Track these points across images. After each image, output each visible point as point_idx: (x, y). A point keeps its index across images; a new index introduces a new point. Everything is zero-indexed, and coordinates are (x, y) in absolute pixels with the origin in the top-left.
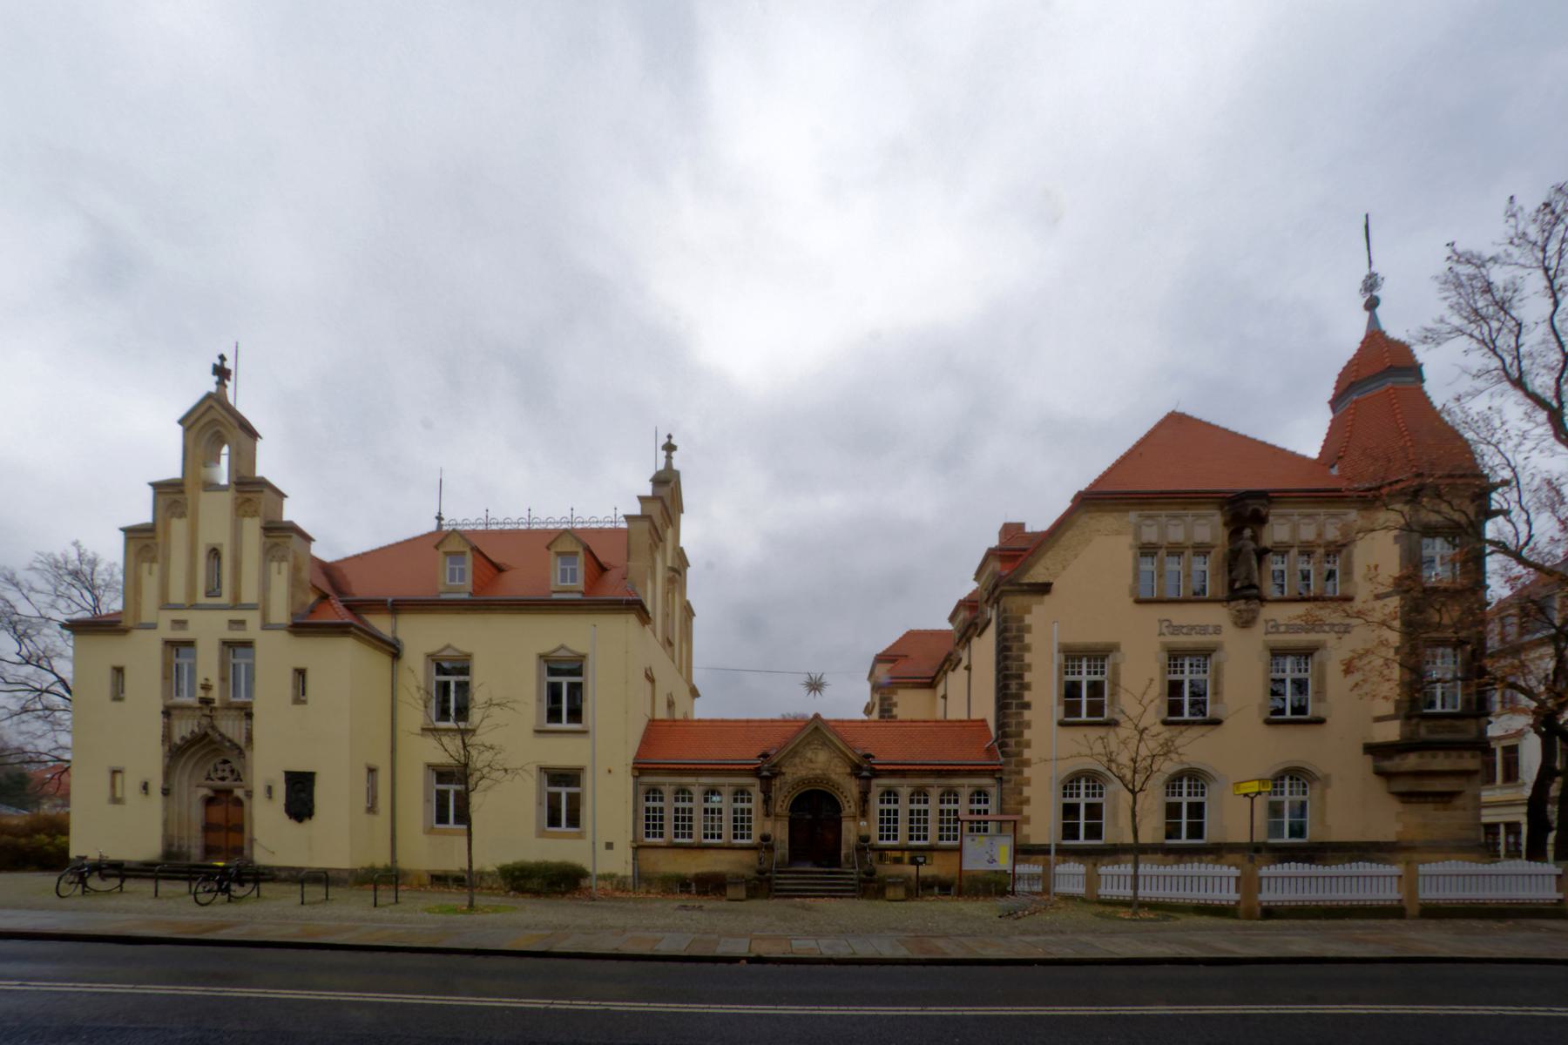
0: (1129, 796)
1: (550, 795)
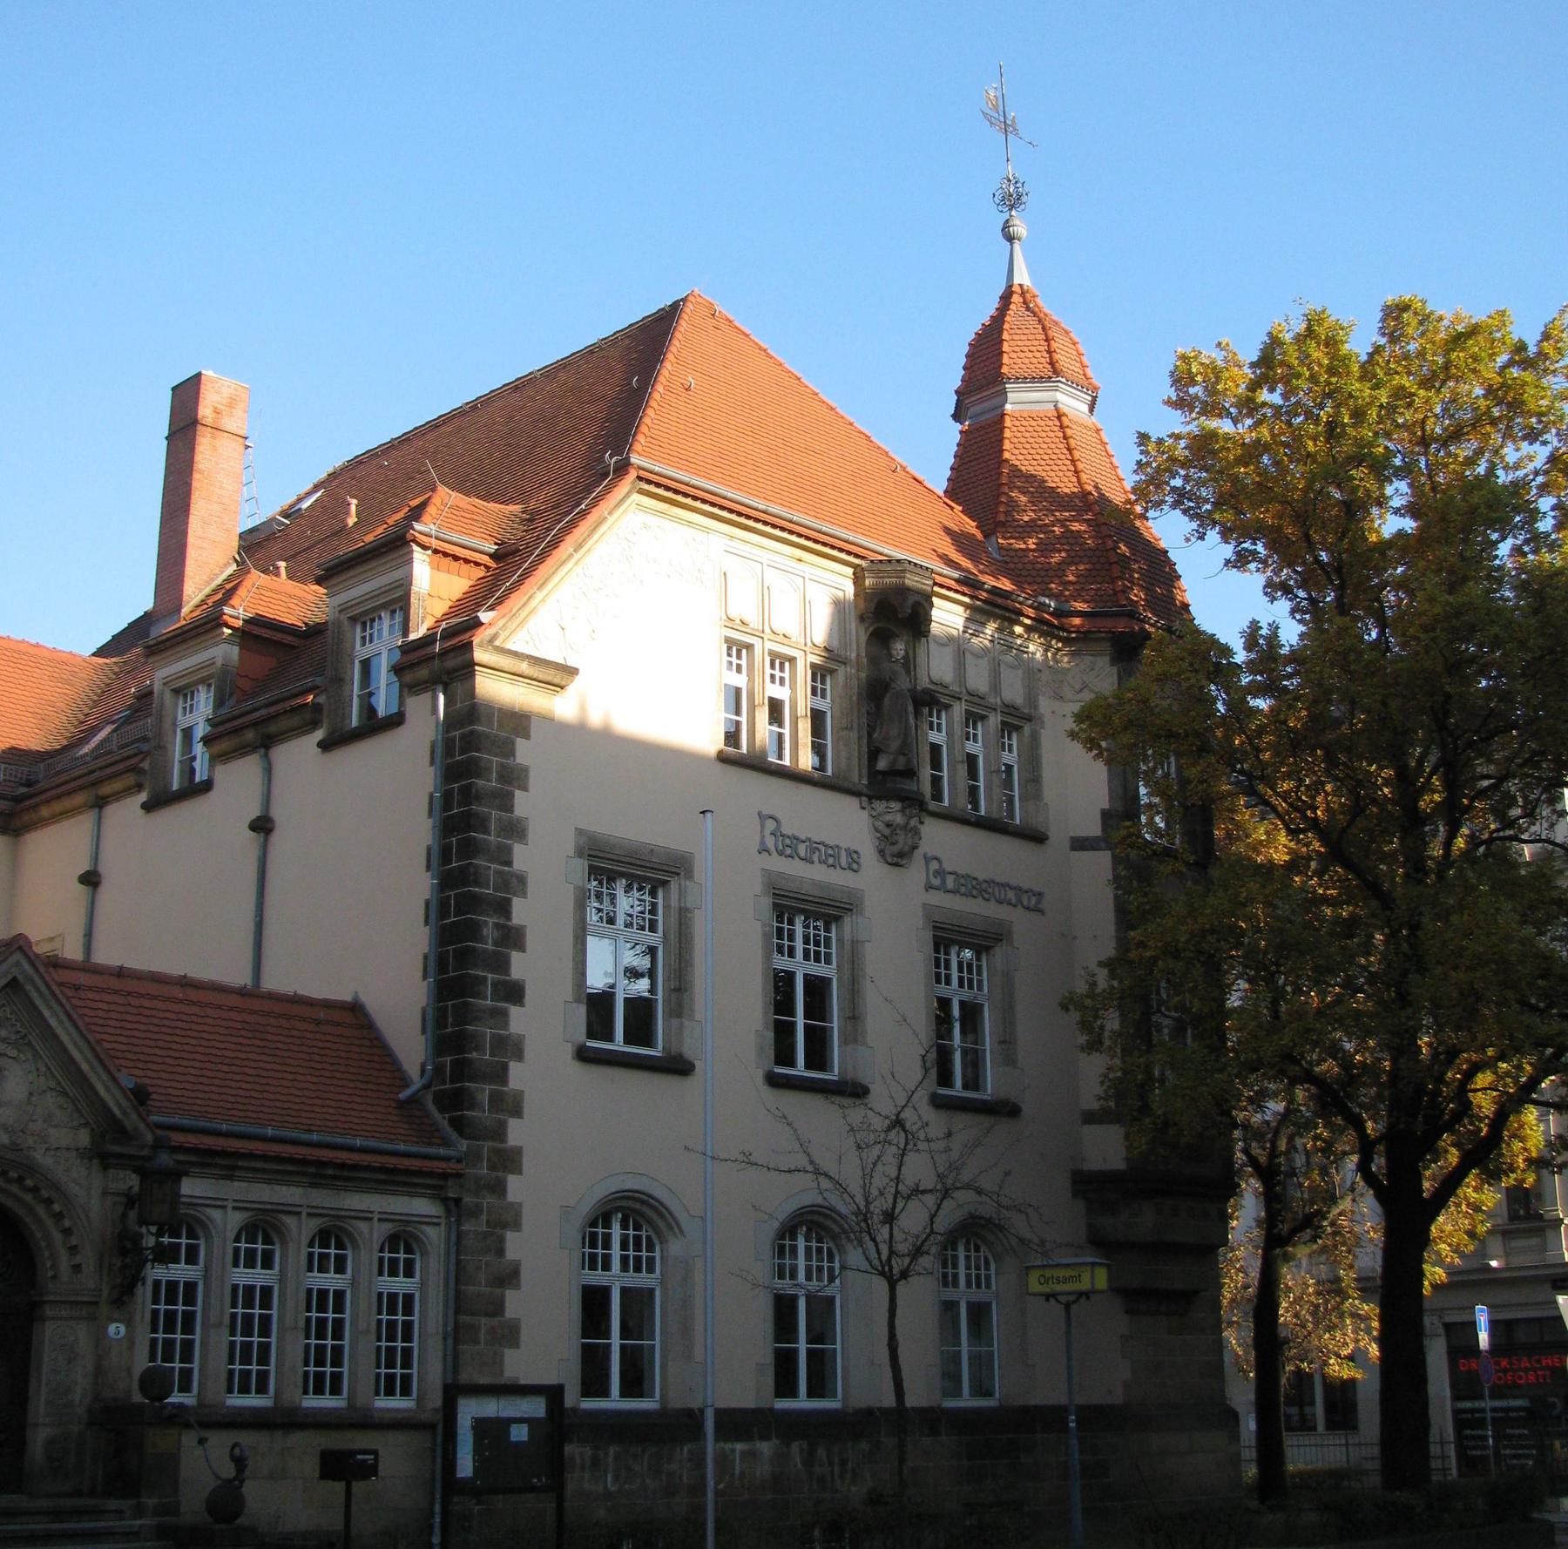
0: (881, 1285)
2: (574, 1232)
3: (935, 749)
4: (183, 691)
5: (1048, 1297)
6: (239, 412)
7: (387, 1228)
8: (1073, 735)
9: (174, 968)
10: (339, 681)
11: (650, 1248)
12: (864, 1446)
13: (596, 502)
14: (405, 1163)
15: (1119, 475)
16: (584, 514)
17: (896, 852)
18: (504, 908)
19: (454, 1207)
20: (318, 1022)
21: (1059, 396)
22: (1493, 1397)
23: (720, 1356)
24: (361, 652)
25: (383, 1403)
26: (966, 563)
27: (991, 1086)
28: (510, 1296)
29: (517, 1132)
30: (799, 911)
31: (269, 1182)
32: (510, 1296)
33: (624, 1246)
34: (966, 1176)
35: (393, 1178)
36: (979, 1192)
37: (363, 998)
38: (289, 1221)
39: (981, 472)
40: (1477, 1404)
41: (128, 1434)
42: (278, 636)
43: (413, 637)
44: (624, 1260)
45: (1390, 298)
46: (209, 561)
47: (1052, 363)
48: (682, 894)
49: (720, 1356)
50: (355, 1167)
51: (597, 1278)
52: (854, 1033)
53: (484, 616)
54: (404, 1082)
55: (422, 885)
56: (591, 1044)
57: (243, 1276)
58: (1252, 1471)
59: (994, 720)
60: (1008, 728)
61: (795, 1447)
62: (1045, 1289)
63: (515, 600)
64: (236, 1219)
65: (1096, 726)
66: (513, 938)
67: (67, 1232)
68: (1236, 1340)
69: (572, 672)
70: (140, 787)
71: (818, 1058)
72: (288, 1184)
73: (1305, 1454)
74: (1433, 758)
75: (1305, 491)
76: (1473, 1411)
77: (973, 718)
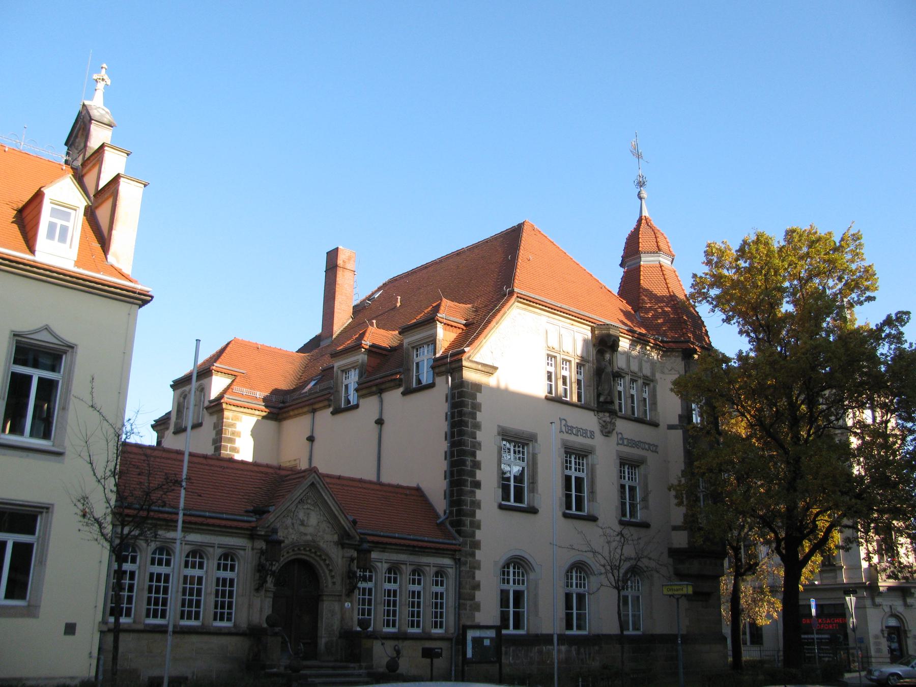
1: (502, 591)
2: (499, 572)
3: (620, 392)
4: (345, 371)
5: (670, 596)
6: (352, 262)
7: (435, 569)
8: (672, 390)
9: (358, 476)
10: (409, 370)
11: (523, 576)
12: (597, 648)
13: (503, 306)
14: (442, 546)
15: (684, 287)
16: (499, 311)
17: (607, 431)
18: (474, 454)
19: (458, 562)
20: (406, 495)
21: (661, 259)
22: (817, 633)
23: (546, 616)
24: (416, 360)
25: (434, 631)
26: (629, 323)
27: (640, 516)
28: (477, 593)
29: (479, 535)
30: (575, 454)
31: (397, 553)
32: (477, 593)
33: (514, 575)
34: (645, 554)
35: (438, 552)
36: (650, 559)
37: (421, 485)
38: (403, 567)
39: (631, 288)
40: (820, 636)
41: (354, 643)
42: (380, 351)
43: (438, 355)
44: (577, 584)
45: (788, 228)
46: (342, 319)
47: (658, 246)
48: (534, 448)
49: (546, 616)
50: (426, 548)
51: (505, 587)
52: (592, 498)
53: (466, 349)
54: (438, 516)
55: (444, 446)
56: (503, 503)
57: (388, 586)
58: (730, 659)
59: (640, 382)
60: (645, 384)
61: (573, 648)
62: (670, 593)
63: (477, 343)
64: (386, 566)
65: (680, 387)
66: (477, 465)
67: (331, 571)
68: (725, 612)
69: (496, 368)
70: (329, 406)
71: (579, 507)
72: (403, 553)
73: (749, 654)
74: (802, 397)
75: (757, 299)
76: (808, 639)
77: (633, 381)
